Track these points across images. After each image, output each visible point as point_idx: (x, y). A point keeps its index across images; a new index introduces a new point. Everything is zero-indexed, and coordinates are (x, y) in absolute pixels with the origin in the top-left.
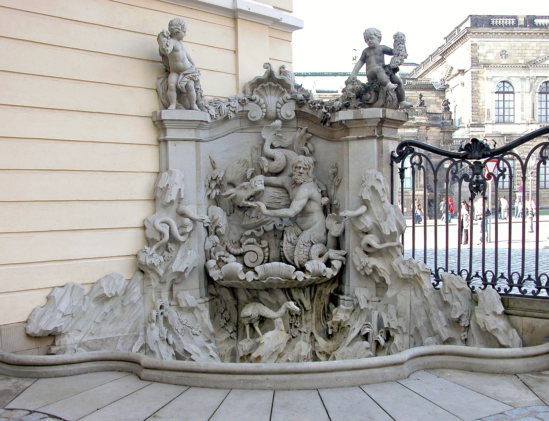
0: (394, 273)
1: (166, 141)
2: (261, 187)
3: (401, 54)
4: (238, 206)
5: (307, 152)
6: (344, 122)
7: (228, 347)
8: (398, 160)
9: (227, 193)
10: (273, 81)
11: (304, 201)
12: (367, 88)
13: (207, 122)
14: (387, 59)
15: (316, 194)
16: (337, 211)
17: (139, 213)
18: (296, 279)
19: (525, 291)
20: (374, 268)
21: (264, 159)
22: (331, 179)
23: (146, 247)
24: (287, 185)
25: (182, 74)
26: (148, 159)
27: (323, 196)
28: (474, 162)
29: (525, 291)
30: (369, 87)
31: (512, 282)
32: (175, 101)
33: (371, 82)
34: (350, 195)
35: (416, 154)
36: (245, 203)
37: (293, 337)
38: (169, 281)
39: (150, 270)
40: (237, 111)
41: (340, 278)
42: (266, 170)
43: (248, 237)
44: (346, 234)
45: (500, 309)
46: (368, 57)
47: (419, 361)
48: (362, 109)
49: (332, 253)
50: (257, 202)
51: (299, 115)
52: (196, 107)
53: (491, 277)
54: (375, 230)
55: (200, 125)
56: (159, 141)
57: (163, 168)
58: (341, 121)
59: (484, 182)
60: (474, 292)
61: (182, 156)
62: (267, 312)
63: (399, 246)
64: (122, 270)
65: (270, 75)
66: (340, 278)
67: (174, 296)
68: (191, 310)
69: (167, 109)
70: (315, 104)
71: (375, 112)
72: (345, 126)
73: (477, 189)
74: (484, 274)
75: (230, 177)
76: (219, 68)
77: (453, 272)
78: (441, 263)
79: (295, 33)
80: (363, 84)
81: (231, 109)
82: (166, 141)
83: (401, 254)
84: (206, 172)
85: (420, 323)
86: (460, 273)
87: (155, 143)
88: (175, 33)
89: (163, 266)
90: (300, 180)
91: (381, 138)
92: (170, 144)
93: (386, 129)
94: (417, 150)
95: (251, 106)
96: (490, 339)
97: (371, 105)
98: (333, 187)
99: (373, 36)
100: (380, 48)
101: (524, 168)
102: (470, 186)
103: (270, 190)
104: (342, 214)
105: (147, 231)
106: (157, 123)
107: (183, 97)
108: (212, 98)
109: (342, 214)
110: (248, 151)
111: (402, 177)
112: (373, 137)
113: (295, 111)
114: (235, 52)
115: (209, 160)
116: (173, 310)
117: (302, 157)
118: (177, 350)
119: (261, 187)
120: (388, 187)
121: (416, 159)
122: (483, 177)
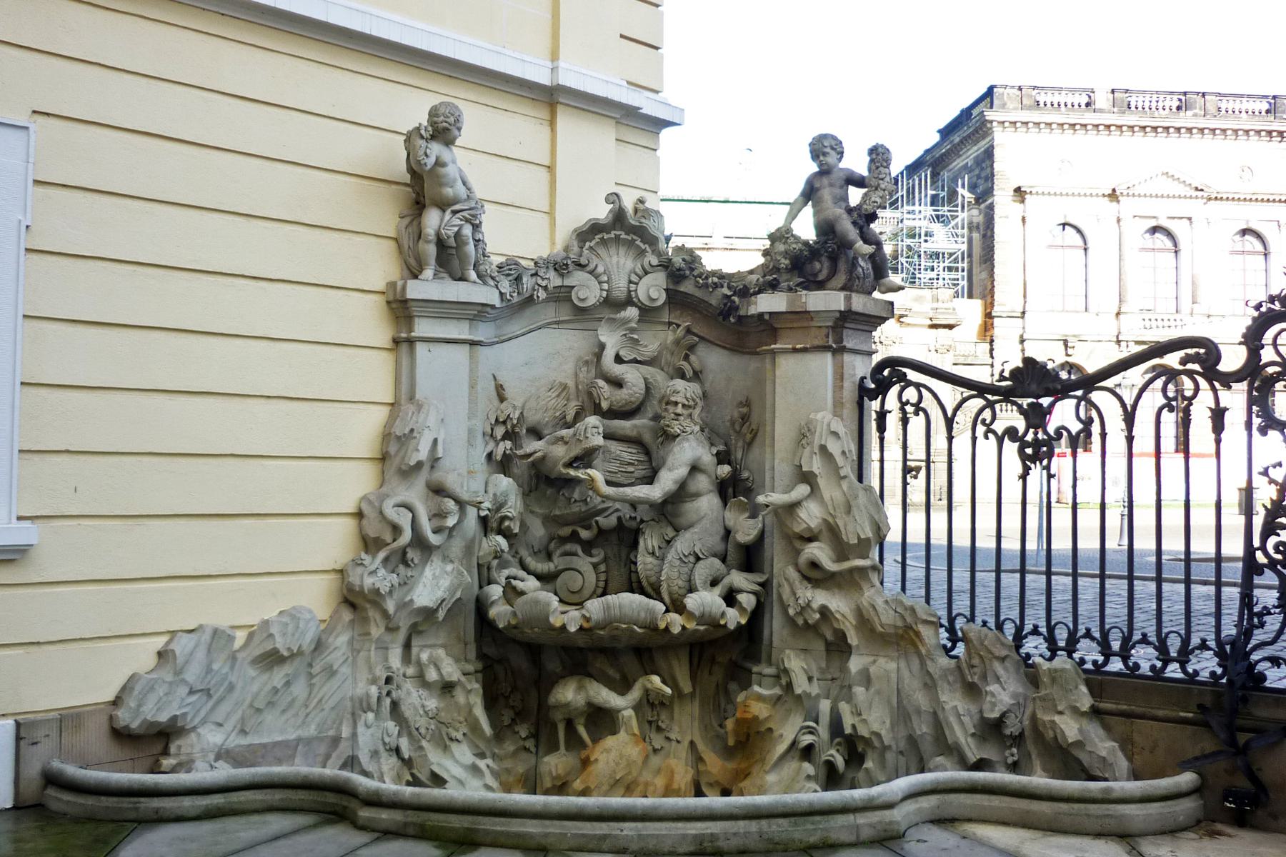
0: (864, 622)
1: (411, 342)
2: (599, 440)
3: (883, 186)
4: (547, 478)
5: (689, 373)
6: (767, 317)
7: (521, 766)
8: (873, 395)
9: (528, 450)
10: (626, 228)
11: (683, 471)
12: (812, 252)
13: (493, 307)
14: (855, 195)
15: (707, 458)
16: (749, 492)
17: (357, 482)
18: (667, 629)
19: (1196, 673)
20: (824, 611)
21: (601, 383)
22: (737, 428)
23: (363, 555)
24: (647, 438)
25: (448, 212)
26: (374, 376)
27: (720, 462)
28: (1029, 405)
29: (1137, 666)
30: (818, 250)
31: (1110, 647)
32: (433, 261)
33: (824, 238)
34: (777, 461)
35: (910, 384)
36: (564, 471)
37: (655, 751)
38: (404, 624)
39: (370, 601)
40: (551, 286)
41: (752, 632)
42: (605, 405)
43: (563, 540)
44: (767, 541)
45: (1086, 702)
46: (818, 190)
47: (928, 803)
48: (804, 292)
49: (738, 579)
50: (589, 471)
51: (675, 299)
52: (473, 275)
53: (1065, 635)
54: (825, 534)
55: (478, 312)
56: (396, 342)
57: (405, 397)
58: (761, 315)
59: (1051, 442)
60: (1033, 666)
61: (441, 368)
62: (607, 697)
63: (874, 568)
64: (315, 599)
65: (619, 217)
66: (752, 632)
67: (413, 658)
68: (447, 688)
69: (416, 277)
70: (707, 278)
71: (828, 301)
72: (770, 326)
73: (1036, 458)
74: (1051, 629)
75: (533, 417)
76: (525, 198)
77: (985, 623)
78: (961, 604)
79: (666, 133)
80: (806, 243)
81: (540, 281)
82: (411, 342)
83: (878, 584)
84: (488, 405)
85: (923, 728)
86: (1000, 626)
87: (389, 345)
88: (442, 130)
89: (395, 596)
90: (676, 429)
91: (839, 350)
92: (420, 348)
93: (850, 332)
94: (912, 375)
95: (578, 278)
96: (1066, 760)
97: (820, 285)
98: (740, 444)
99: (828, 150)
100: (841, 174)
101: (1129, 418)
102: (1021, 451)
103: (614, 446)
104: (761, 499)
105: (364, 522)
106: (394, 306)
107: (450, 257)
108: (503, 259)
109: (761, 499)
110: (569, 367)
111: (882, 428)
112: (825, 348)
113: (667, 290)
114: (551, 168)
115: (493, 383)
116: (409, 685)
117: (679, 384)
118: (415, 771)
119: (599, 440)
120: (853, 448)
121: (911, 394)
122: (1046, 432)
